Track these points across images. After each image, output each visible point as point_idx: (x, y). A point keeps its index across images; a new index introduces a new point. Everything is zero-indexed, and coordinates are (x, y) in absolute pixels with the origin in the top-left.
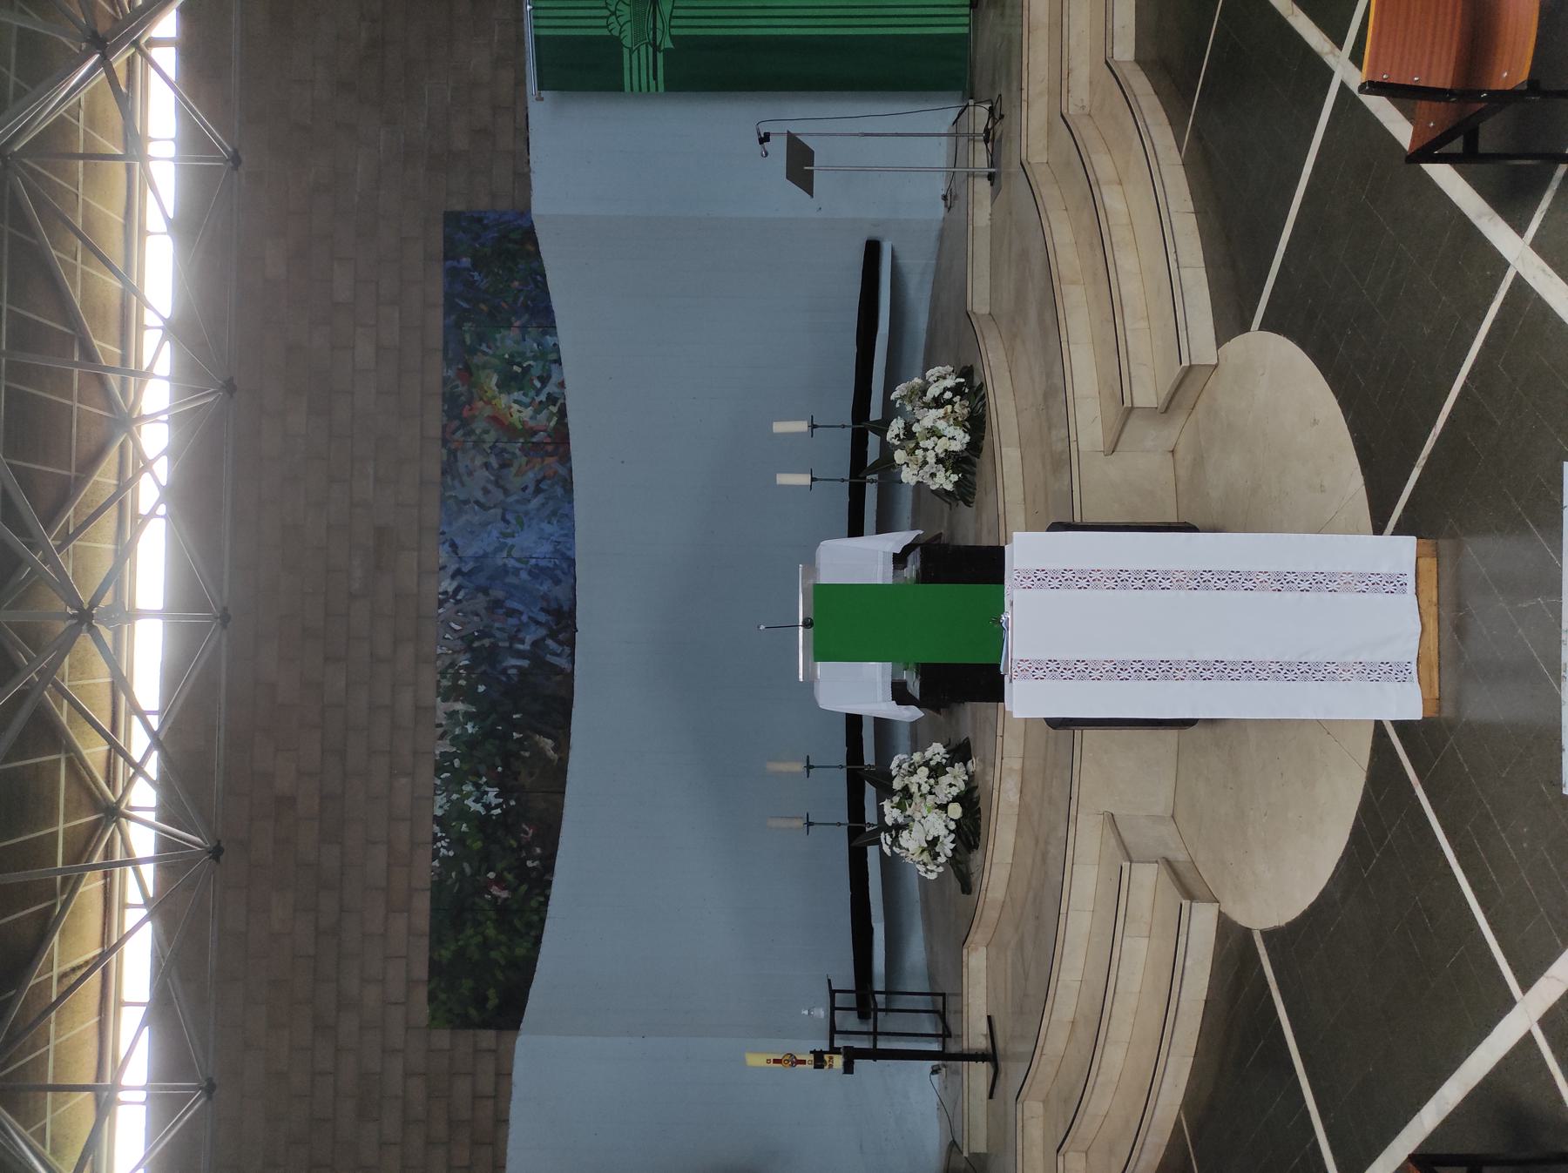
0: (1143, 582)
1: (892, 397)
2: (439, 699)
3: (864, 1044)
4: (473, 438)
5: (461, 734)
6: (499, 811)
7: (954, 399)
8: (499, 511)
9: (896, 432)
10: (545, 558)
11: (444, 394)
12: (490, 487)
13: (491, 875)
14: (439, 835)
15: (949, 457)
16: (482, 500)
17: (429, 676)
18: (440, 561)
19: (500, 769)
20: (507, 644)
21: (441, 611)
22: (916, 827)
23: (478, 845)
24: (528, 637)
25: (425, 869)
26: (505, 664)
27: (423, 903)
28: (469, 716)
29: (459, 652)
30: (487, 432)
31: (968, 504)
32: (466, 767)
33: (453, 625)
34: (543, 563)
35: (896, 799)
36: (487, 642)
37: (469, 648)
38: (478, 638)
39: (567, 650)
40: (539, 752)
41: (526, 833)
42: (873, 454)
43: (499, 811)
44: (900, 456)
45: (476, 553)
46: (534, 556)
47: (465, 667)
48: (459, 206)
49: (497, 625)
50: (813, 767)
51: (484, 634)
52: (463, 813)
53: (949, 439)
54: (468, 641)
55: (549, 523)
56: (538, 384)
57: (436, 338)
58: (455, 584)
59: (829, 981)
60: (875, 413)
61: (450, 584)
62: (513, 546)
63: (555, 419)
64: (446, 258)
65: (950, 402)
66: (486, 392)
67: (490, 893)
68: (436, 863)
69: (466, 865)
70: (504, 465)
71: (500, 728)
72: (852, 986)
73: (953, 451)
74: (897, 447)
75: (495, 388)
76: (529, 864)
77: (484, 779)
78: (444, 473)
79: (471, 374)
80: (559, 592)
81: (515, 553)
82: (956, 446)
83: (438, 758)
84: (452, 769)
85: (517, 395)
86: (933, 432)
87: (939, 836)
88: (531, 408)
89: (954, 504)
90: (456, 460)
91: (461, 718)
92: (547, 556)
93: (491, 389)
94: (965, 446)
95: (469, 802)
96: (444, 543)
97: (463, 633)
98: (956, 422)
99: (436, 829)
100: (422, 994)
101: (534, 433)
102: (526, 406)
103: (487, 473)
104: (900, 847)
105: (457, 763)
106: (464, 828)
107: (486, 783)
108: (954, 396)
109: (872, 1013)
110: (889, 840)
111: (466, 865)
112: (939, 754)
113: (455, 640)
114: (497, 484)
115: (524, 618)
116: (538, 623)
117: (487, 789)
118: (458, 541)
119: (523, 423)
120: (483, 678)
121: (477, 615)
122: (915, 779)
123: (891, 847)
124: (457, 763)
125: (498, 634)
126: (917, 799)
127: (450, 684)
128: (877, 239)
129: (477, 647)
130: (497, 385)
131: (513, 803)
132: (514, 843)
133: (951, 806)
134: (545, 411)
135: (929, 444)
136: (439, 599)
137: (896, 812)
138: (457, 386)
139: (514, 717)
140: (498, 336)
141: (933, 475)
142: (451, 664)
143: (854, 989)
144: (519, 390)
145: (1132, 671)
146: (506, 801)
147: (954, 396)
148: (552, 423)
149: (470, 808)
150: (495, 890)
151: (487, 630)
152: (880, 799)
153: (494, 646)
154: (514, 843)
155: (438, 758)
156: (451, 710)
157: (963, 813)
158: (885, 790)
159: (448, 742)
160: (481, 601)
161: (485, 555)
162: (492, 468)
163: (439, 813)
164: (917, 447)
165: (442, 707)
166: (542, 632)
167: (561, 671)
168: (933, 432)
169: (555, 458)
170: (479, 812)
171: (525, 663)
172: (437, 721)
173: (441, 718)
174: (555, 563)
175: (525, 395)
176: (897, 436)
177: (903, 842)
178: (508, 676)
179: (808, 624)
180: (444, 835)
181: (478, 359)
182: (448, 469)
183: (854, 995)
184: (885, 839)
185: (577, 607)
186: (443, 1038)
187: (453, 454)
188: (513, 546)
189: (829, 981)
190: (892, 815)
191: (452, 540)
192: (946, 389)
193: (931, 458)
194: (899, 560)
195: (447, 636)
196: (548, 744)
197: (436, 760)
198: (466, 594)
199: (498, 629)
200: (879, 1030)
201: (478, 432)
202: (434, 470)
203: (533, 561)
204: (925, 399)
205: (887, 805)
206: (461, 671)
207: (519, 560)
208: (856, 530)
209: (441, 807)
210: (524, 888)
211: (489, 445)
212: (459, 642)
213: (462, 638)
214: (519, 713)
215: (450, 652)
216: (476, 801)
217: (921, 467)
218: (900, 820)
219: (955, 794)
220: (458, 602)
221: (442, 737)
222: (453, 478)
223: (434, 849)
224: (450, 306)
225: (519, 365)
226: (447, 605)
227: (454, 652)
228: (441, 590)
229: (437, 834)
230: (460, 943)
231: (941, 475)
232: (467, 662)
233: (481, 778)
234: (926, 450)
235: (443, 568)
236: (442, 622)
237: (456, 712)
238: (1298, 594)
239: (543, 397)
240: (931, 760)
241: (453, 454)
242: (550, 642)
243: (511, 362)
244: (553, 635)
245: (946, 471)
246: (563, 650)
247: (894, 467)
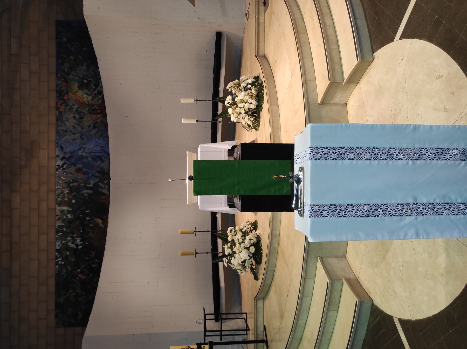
0: (371, 155)
1: (227, 88)
2: (57, 206)
3: (217, 339)
4: (69, 107)
5: (66, 219)
6: (81, 247)
7: (252, 88)
8: (80, 135)
9: (229, 101)
10: (98, 152)
11: (57, 90)
12: (76, 126)
13: (79, 270)
14: (58, 256)
15: (250, 111)
16: (73, 130)
17: (52, 197)
18: (56, 154)
19: (81, 231)
20: (83, 185)
21: (57, 172)
22: (237, 255)
23: (73, 259)
24: (92, 182)
25: (52, 269)
26: (82, 192)
27: (52, 282)
28: (69, 212)
29: (64, 188)
30: (74, 105)
31: (256, 129)
32: (68, 231)
33: (62, 177)
34: (97, 154)
35: (229, 245)
36: (75, 184)
37: (69, 186)
38: (72, 183)
39: (107, 187)
40: (97, 225)
41: (92, 254)
42: (220, 111)
43: (81, 247)
44: (230, 111)
45: (70, 151)
46: (93, 152)
47: (68, 193)
48: (61, 18)
49: (79, 178)
50: (197, 232)
51: (74, 181)
52: (68, 248)
53: (250, 103)
54: (68, 184)
55: (99, 139)
56: (94, 87)
57: (53, 69)
58: (62, 162)
59: (204, 309)
60: (221, 95)
61: (60, 162)
62: (85, 148)
63: (101, 100)
64: (57, 38)
65: (250, 89)
66: (73, 90)
67: (78, 277)
68: (57, 267)
69: (69, 267)
70: (81, 118)
71: (81, 216)
72: (213, 312)
73: (251, 109)
74: (229, 107)
75: (77, 88)
76: (93, 266)
77: (75, 235)
78: (57, 120)
79: (67, 83)
80: (104, 165)
81: (86, 151)
82: (253, 107)
83: (57, 228)
84: (62, 232)
85: (85, 91)
86: (242, 101)
87: (246, 259)
88: (91, 96)
89: (250, 131)
90: (62, 115)
91: (66, 212)
92: (99, 152)
93: (75, 88)
94: (256, 107)
95: (70, 244)
96: (58, 147)
97: (66, 181)
98: (251, 97)
99: (57, 254)
100: (52, 315)
101: (93, 106)
102: (90, 95)
103: (74, 121)
104: (231, 264)
105: (64, 229)
106: (68, 253)
107: (76, 237)
108: (252, 86)
109: (220, 320)
110: (227, 261)
111: (69, 267)
112: (246, 227)
113: (63, 183)
114: (78, 125)
115: (90, 175)
116: (95, 177)
117: (77, 239)
118: (63, 146)
119: (88, 101)
120: (75, 197)
121: (72, 174)
122: (237, 237)
123: (227, 264)
124: (64, 229)
125: (80, 181)
126: (237, 244)
127: (61, 200)
128: (221, 32)
129: (72, 186)
130: (78, 87)
131: (87, 243)
132: (87, 258)
133: (251, 248)
134: (97, 98)
135: (241, 105)
136: (56, 168)
137: (229, 250)
138: (62, 87)
139: (87, 211)
140: (78, 68)
141: (243, 118)
142: (62, 192)
143: (214, 313)
144: (87, 89)
145: (381, 211)
146: (84, 243)
147: (252, 86)
148: (100, 102)
149: (70, 246)
150: (80, 276)
151: (75, 179)
152: (223, 245)
153: (79, 186)
154: (87, 258)
155: (57, 228)
156: (62, 209)
157: (255, 250)
158: (225, 241)
159: (61, 221)
160: (73, 169)
161: (74, 151)
162: (77, 119)
163: (58, 248)
164: (237, 106)
165: (58, 208)
166: (98, 180)
167: (104, 194)
168: (242, 101)
169: (101, 115)
170: (74, 247)
171: (91, 192)
172: (57, 214)
173: (58, 213)
174: (102, 154)
175: (89, 91)
176: (229, 103)
177: (232, 262)
178: (84, 197)
179: (190, 178)
180: (60, 256)
181: (71, 77)
182: (59, 118)
183: (214, 315)
184: (225, 261)
185: (110, 171)
186: (61, 331)
187: (61, 113)
188: (85, 148)
189: (204, 309)
190: (228, 251)
191: (61, 146)
192: (249, 84)
193: (243, 112)
194: (231, 152)
195: (60, 182)
196: (100, 221)
197: (56, 229)
198: (67, 166)
199: (80, 179)
200: (223, 329)
201: (71, 104)
202: (53, 119)
203: (93, 154)
204: (240, 88)
205: (226, 247)
206: (66, 195)
207: (87, 153)
208: (214, 140)
209: (59, 246)
210: (92, 274)
211: (75, 110)
212: (64, 184)
213: (66, 183)
214: (88, 210)
215: (61, 188)
216: (72, 243)
217: (239, 115)
218: (231, 253)
219: (252, 243)
220: (64, 169)
221: (58, 220)
222: (61, 122)
223: (56, 262)
224: (58, 57)
225: (86, 79)
226: (60, 170)
227: (63, 188)
228: (57, 164)
229: (57, 256)
230: (67, 296)
231: (246, 118)
232: (68, 192)
233: (74, 235)
234: (241, 108)
235: (58, 156)
236: (58, 176)
237: (64, 210)
238: (444, 162)
239: (96, 92)
240: (243, 229)
241: (61, 113)
242: (100, 184)
243: (83, 79)
244: (101, 181)
245: (248, 116)
246: (105, 187)
247: (228, 115)
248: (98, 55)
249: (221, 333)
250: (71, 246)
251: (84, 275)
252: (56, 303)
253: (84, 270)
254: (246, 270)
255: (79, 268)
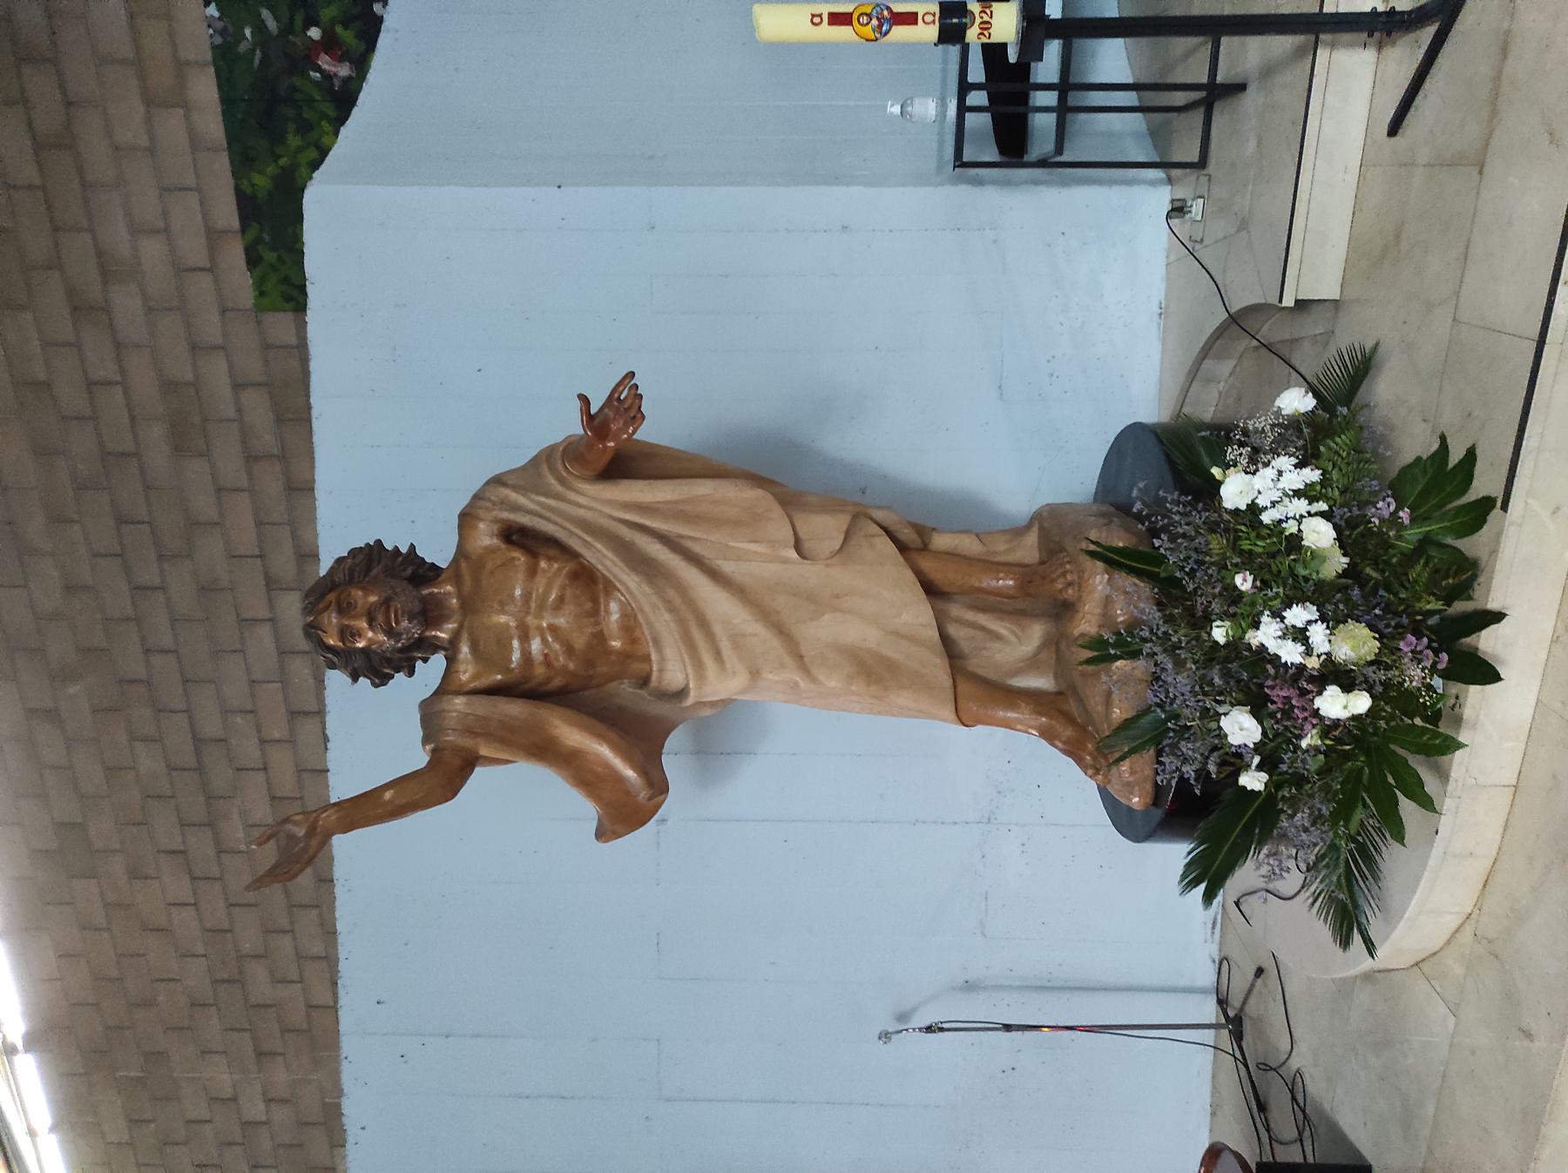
13: (314, 33)
27: (205, 89)
67: (319, 69)
150: (325, 62)
207: (1164, 747)
230: (283, 161)
248: (1050, 973)
249: (1062, 99)
250: (1309, 431)
251: (341, 59)
252: (240, 194)
253: (339, 29)
254: (1312, 910)
255: (311, 21)
